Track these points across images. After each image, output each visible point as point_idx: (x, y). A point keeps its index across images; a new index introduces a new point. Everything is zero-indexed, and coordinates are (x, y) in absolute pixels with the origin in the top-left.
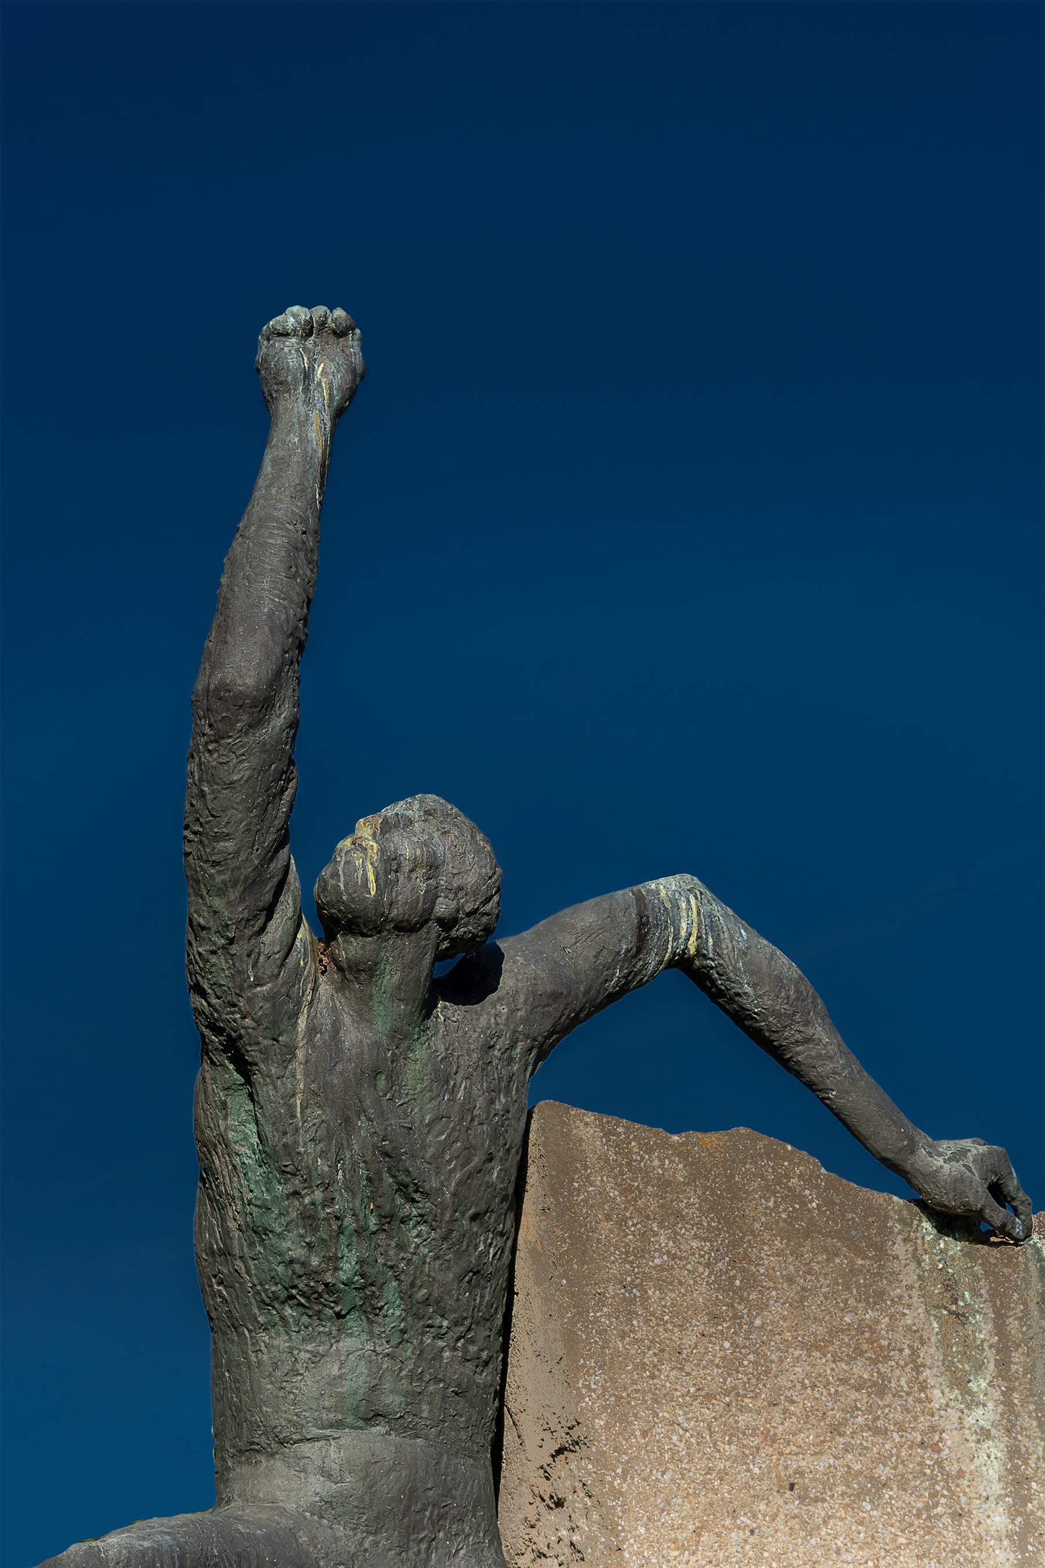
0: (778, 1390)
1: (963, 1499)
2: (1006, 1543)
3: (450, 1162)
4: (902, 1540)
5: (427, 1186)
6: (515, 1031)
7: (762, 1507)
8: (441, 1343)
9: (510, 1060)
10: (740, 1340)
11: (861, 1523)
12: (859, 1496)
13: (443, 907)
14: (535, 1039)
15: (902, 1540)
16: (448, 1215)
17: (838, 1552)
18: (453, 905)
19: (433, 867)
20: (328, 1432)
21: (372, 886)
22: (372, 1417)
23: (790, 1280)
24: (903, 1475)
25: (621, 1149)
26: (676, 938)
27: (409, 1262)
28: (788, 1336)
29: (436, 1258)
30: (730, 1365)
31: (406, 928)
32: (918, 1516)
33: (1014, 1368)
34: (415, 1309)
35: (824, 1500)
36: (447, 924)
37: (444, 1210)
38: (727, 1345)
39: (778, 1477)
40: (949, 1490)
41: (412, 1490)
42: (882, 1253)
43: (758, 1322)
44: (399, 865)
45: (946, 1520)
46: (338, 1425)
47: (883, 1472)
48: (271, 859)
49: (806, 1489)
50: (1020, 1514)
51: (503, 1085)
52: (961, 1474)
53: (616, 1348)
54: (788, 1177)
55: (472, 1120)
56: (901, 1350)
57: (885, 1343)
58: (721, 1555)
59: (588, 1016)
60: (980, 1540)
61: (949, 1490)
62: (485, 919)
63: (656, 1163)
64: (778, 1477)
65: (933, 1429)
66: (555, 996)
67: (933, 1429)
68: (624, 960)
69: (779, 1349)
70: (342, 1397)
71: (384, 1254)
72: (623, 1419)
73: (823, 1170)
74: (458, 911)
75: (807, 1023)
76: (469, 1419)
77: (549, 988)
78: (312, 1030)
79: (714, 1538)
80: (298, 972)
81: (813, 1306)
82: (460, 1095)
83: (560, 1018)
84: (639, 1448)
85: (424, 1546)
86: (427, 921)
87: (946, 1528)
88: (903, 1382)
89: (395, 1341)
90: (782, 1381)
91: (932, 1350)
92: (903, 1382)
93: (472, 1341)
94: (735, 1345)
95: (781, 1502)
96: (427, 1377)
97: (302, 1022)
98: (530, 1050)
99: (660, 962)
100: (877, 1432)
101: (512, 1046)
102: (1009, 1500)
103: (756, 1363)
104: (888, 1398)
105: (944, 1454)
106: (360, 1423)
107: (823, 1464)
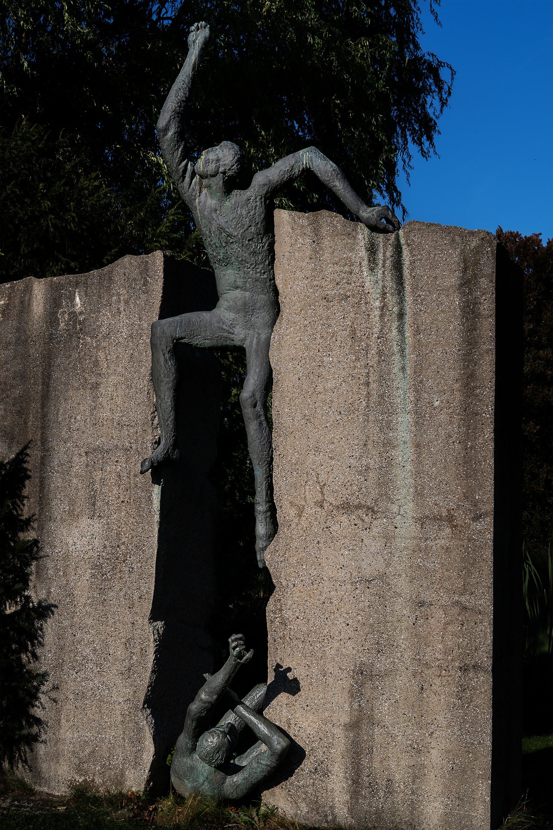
0: (325, 275)
1: (368, 299)
2: (378, 309)
3: (239, 228)
4: (351, 310)
5: (234, 235)
6: (256, 195)
7: (317, 304)
8: (249, 270)
9: (256, 202)
10: (316, 264)
11: (341, 306)
12: (342, 299)
13: (221, 169)
14: (261, 196)
15: (351, 310)
16: (241, 241)
17: (335, 314)
18: (223, 168)
19: (218, 160)
20: (228, 292)
21: (201, 167)
22: (237, 288)
23: (331, 247)
24: (353, 294)
25: (293, 219)
26: (303, 164)
27: (235, 252)
28: (329, 261)
29: (242, 251)
30: (314, 270)
31: (214, 176)
32: (356, 304)
33: (386, 265)
34: (241, 262)
35: (333, 301)
36: (224, 173)
37: (240, 240)
38: (313, 265)
39: (322, 296)
40: (365, 297)
41: (245, 304)
42: (355, 238)
43: (321, 259)
44: (209, 161)
45: (363, 304)
46: (229, 290)
47: (349, 294)
48: (180, 165)
49: (328, 299)
50: (383, 302)
51: (253, 208)
52: (369, 293)
53: (286, 268)
54: (333, 221)
55: (243, 218)
56: (357, 263)
57: (353, 261)
58: (306, 316)
59: (404, 166)
60: (371, 309)
61: (365, 297)
62: (233, 170)
63: (301, 221)
64: (322, 296)
65: (363, 282)
66: (265, 185)
67: (363, 282)
68: (287, 172)
69: (326, 265)
70: (229, 284)
71: (229, 251)
72: (286, 285)
73: (343, 219)
74: (225, 170)
75: (333, 182)
76: (261, 286)
77: (263, 183)
78: (199, 202)
79: (305, 312)
80: (193, 190)
81: (336, 254)
82: (239, 212)
83: (268, 189)
84: (289, 291)
85: (250, 316)
86: (218, 173)
87: (363, 306)
88: (357, 271)
89: (238, 270)
90: (326, 273)
91: (365, 262)
92: (357, 271)
93: (257, 268)
94: (315, 265)
95: (322, 302)
96: (247, 278)
97: (197, 200)
98: (262, 198)
99: (299, 171)
100: (348, 284)
101: (256, 198)
102: (380, 299)
103: (320, 269)
104: (352, 275)
105: (365, 288)
106: (234, 289)
107: (333, 293)
